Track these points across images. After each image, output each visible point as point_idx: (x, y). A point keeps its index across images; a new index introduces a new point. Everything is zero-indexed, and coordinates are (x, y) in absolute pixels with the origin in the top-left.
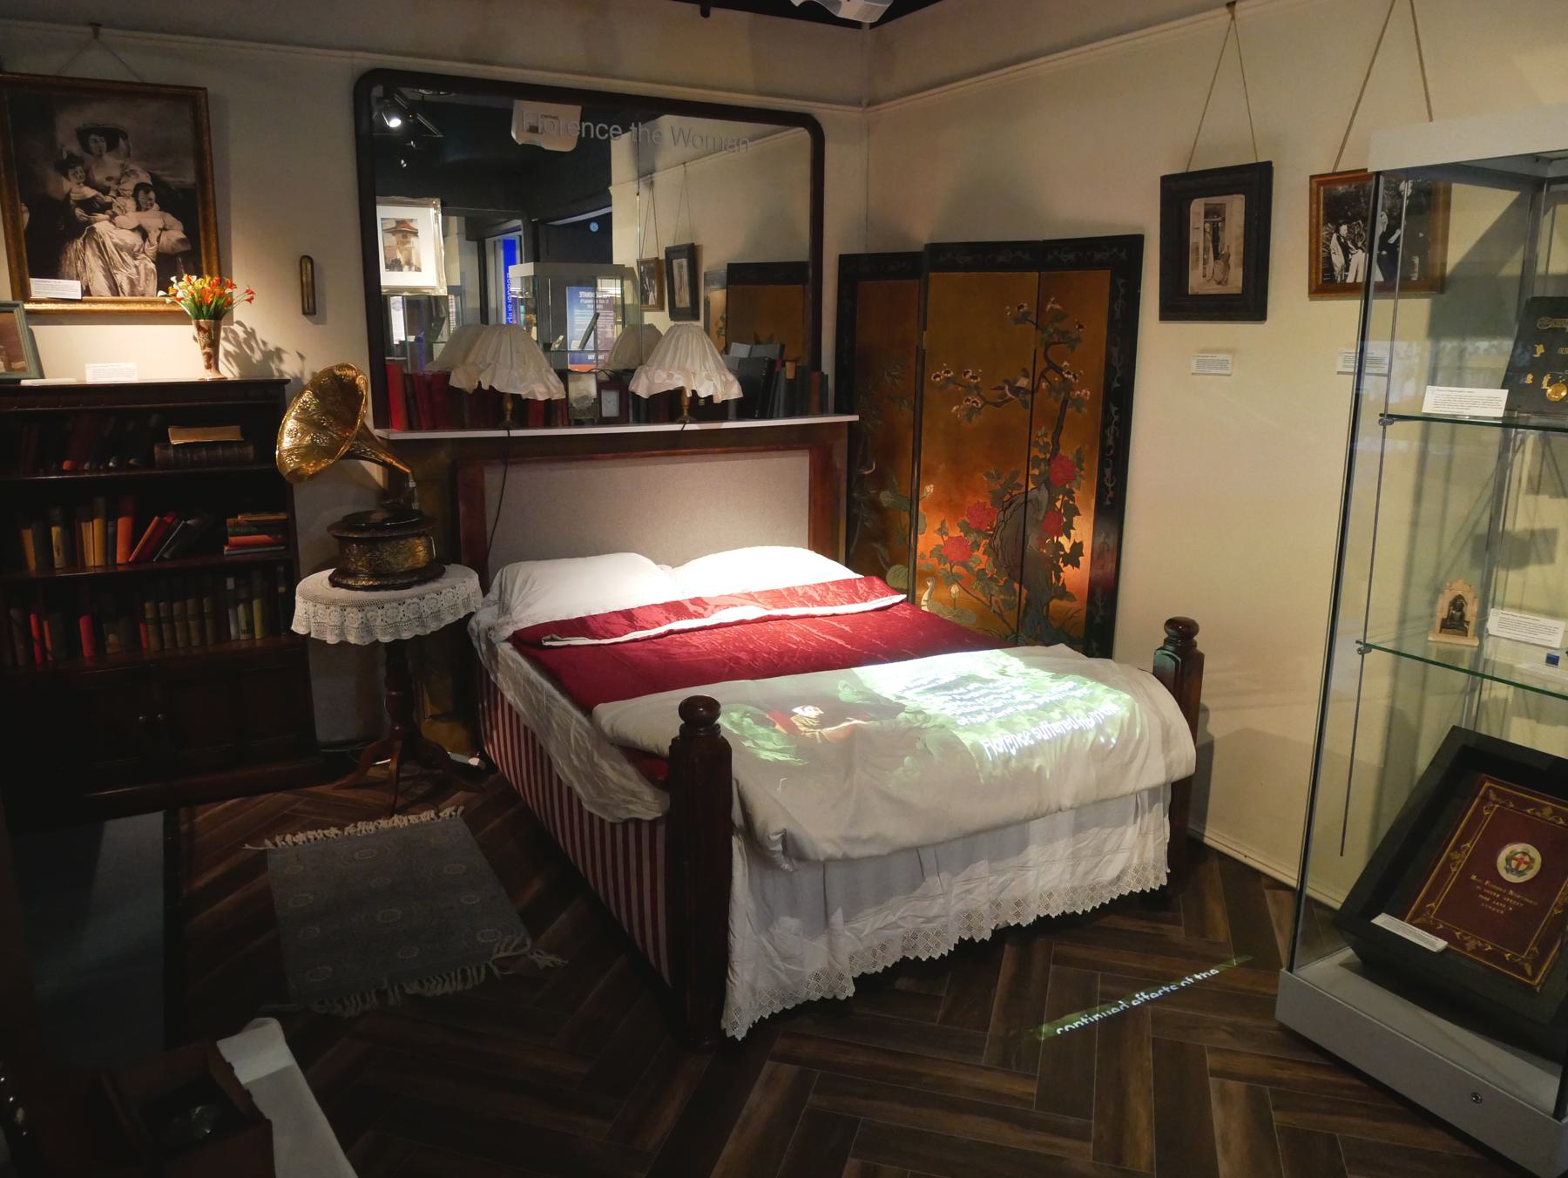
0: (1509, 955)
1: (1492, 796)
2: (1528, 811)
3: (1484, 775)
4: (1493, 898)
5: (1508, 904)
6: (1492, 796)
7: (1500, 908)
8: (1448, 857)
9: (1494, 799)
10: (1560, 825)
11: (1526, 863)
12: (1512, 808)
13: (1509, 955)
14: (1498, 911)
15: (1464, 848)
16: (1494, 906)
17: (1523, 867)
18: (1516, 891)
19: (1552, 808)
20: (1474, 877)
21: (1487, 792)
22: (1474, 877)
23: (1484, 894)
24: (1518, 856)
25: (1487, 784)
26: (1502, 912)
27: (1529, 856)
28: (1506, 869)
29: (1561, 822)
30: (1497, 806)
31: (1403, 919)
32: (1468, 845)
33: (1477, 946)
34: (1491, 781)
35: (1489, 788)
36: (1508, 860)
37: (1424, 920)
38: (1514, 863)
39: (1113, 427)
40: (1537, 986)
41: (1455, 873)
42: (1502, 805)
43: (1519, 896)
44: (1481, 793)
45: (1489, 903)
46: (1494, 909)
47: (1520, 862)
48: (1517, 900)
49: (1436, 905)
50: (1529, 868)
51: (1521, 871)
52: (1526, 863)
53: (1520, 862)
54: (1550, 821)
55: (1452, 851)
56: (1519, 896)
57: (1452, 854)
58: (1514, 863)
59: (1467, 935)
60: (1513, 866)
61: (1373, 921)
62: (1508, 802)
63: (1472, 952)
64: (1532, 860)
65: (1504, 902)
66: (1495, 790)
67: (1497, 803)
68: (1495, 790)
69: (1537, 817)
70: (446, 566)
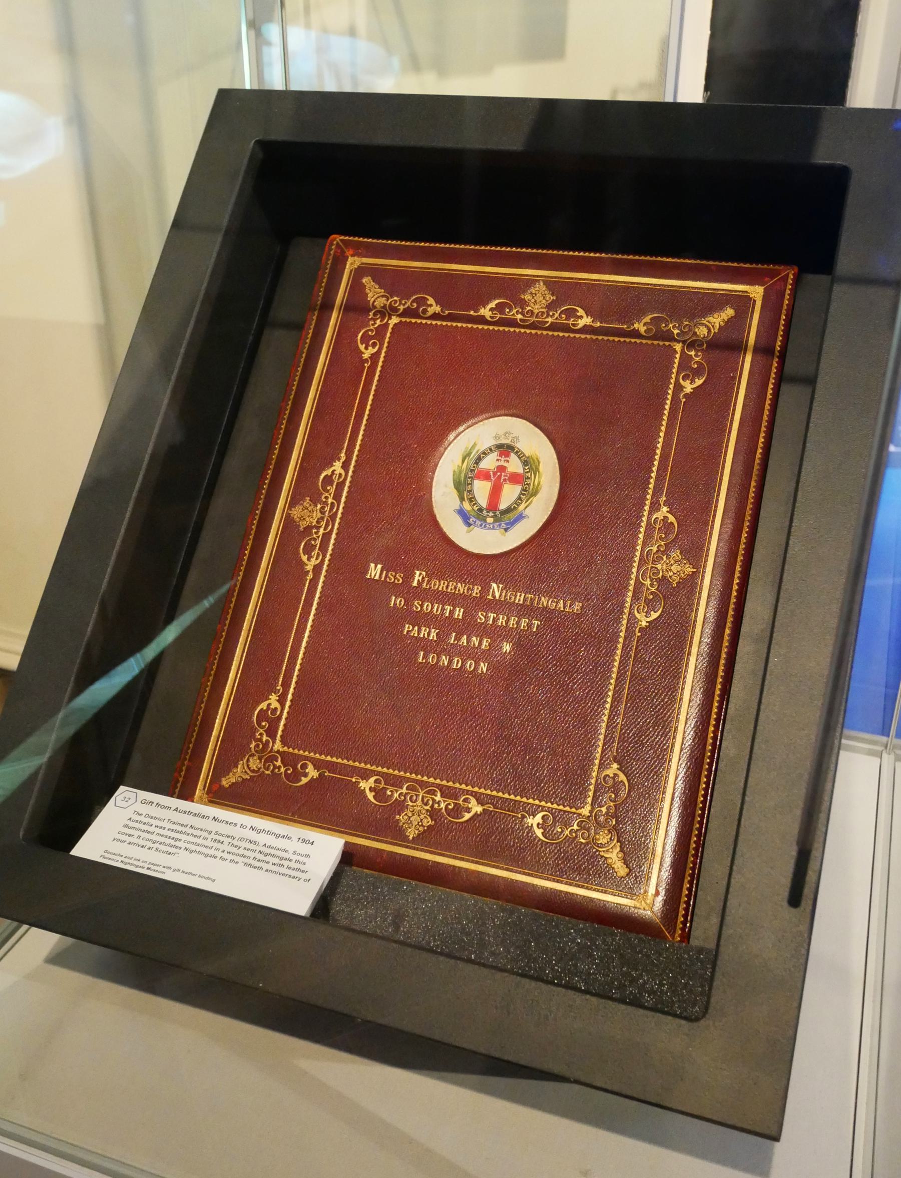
0: (538, 818)
1: (375, 294)
2: (640, 327)
3: (338, 239)
4: (446, 625)
5: (496, 633)
6: (375, 294)
7: (476, 655)
8: (289, 523)
9: (381, 302)
10: (586, 329)
11: (515, 479)
12: (435, 316)
13: (538, 818)
14: (470, 665)
15: (328, 480)
16: (452, 651)
17: (510, 494)
18: (509, 583)
19: (551, 285)
20: (375, 571)
21: (356, 287)
22: (375, 571)
23: (419, 619)
24: (490, 463)
25: (353, 262)
26: (483, 667)
27: (520, 455)
28: (461, 512)
29: (586, 321)
30: (395, 320)
31: (187, 795)
32: (337, 466)
33: (433, 813)
34: (359, 250)
35: (360, 272)
36: (462, 486)
37: (255, 763)
38: (482, 490)
39: (657, 527)
40: (473, 587)
41: (317, 569)
42: (407, 313)
43: (520, 598)
44: (341, 296)
45: (439, 646)
46: (457, 663)
47: (498, 479)
48: (526, 610)
49: (282, 701)
50: (528, 493)
51: (509, 510)
52: (515, 479)
53: (498, 479)
54: (554, 327)
55: (294, 501)
56: (520, 598)
57: (296, 512)
58: (482, 490)
59: (397, 782)
60: (483, 501)
61: (75, 852)
62: (422, 301)
63: (425, 839)
64: (529, 463)
65: (484, 631)
66: (377, 274)
67: (393, 310)
68: (377, 274)
69: (512, 323)
70: (763, 287)
